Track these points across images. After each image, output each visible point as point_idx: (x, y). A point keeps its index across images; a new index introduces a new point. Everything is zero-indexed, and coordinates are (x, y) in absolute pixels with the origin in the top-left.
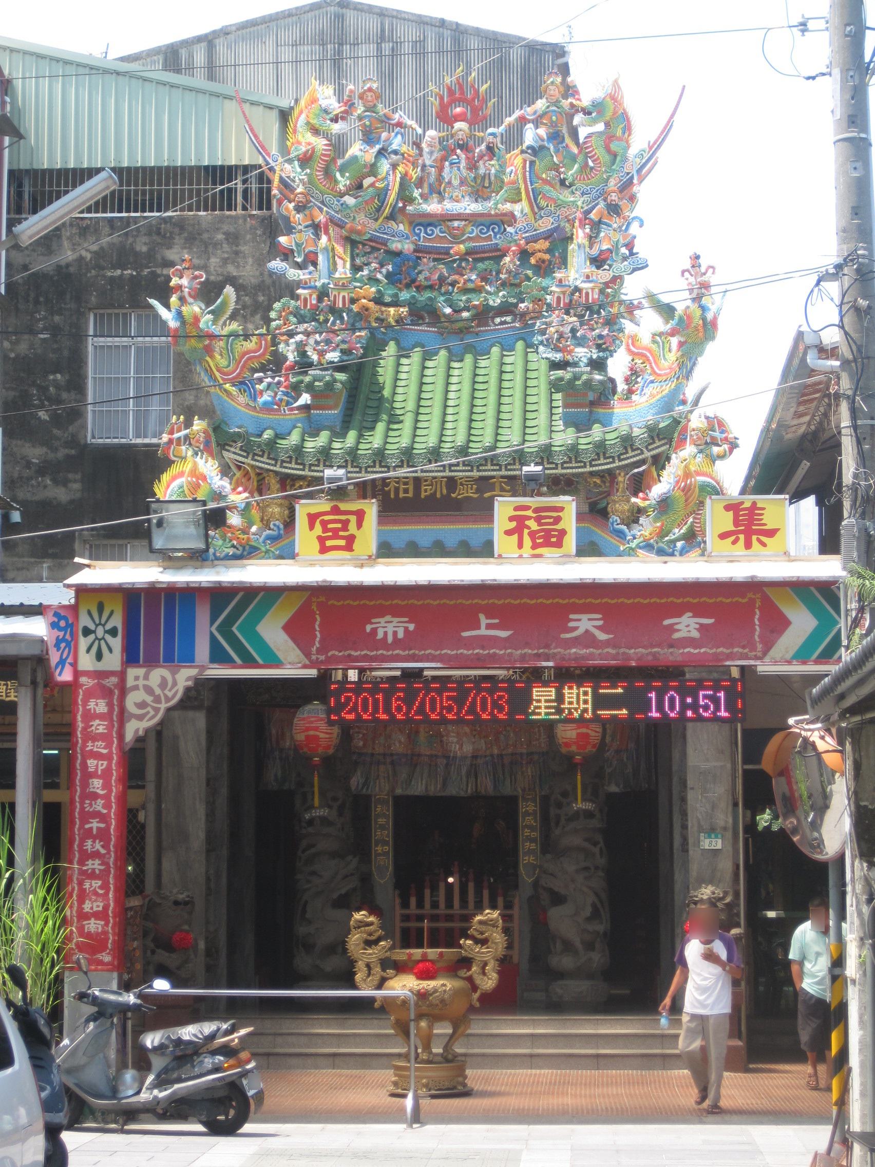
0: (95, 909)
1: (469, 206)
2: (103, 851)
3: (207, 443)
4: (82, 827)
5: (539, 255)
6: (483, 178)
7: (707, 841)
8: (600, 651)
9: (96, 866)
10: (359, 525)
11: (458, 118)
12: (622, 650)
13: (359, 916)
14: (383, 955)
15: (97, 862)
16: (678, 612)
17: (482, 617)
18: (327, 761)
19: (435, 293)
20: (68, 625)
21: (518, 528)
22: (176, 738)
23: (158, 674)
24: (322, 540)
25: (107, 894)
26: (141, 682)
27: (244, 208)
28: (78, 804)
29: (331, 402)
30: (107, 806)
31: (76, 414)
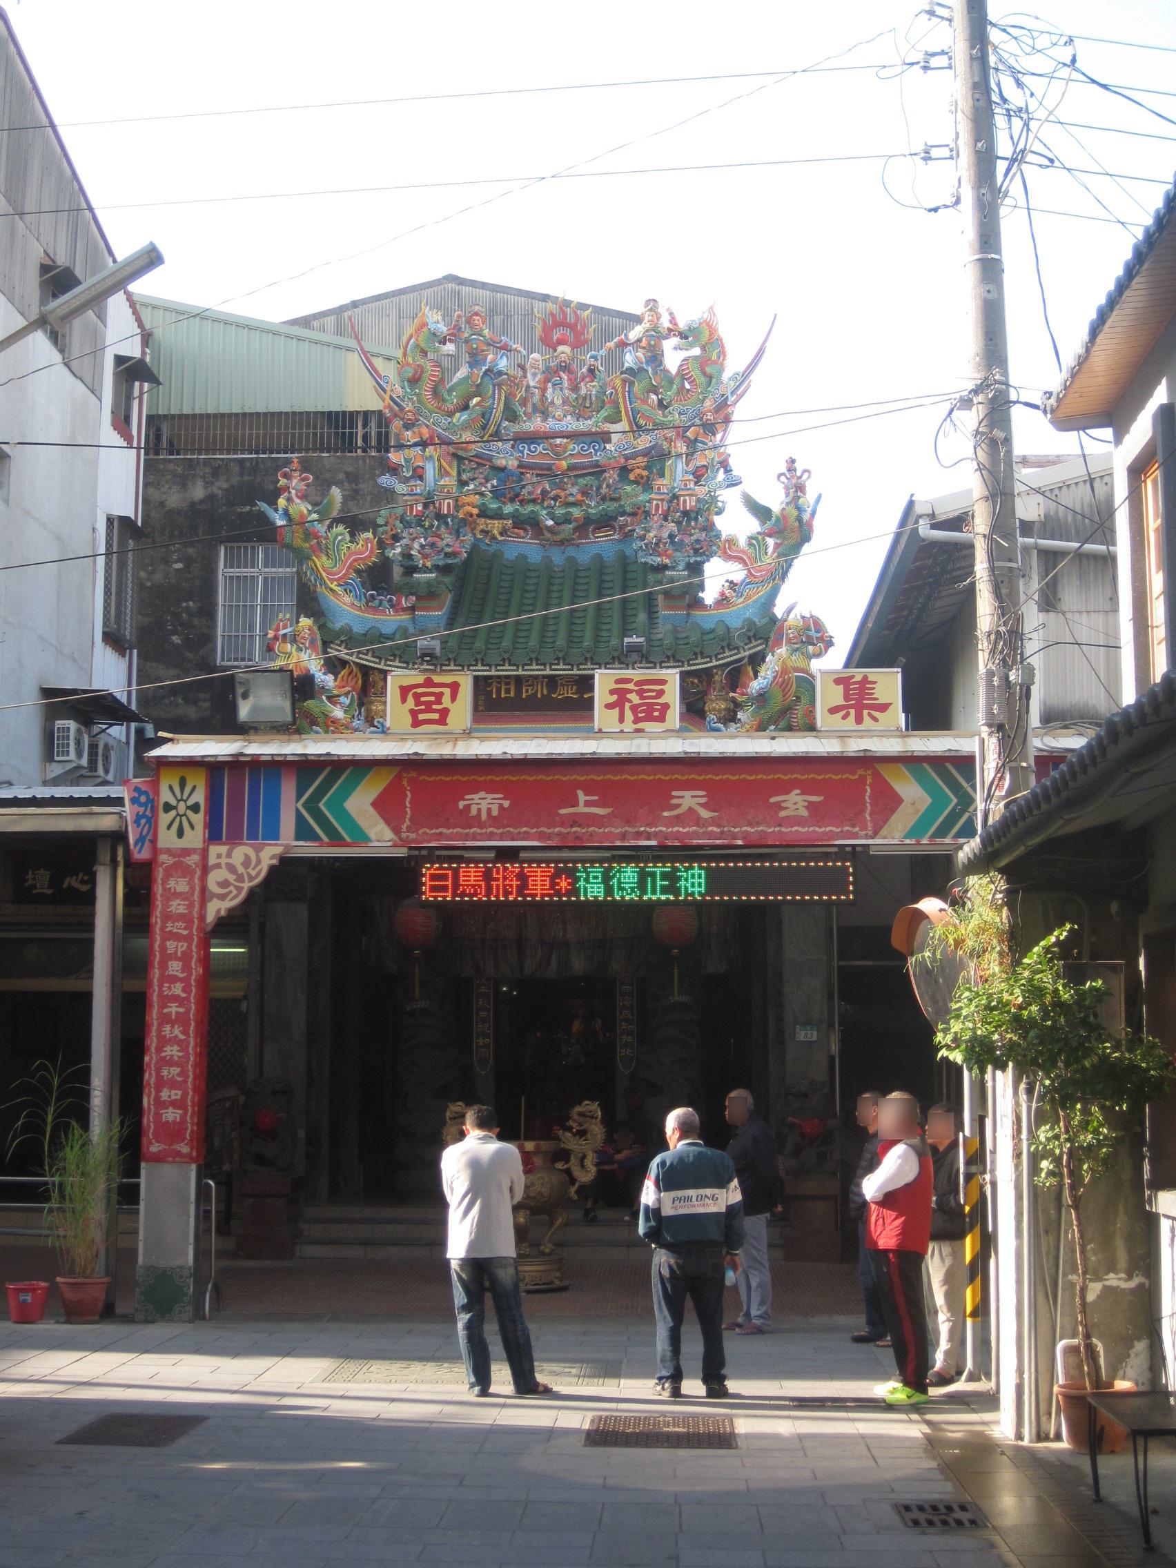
1: (571, 424)
3: (313, 643)
4: (160, 1013)
5: (638, 471)
6: (585, 398)
7: (803, 1033)
9: (175, 1053)
10: (453, 698)
11: (561, 342)
16: (786, 788)
17: (580, 793)
21: (619, 701)
23: (241, 852)
24: (414, 713)
25: (185, 1082)
26: (224, 861)
27: (364, 451)
29: (435, 604)
31: (207, 638)
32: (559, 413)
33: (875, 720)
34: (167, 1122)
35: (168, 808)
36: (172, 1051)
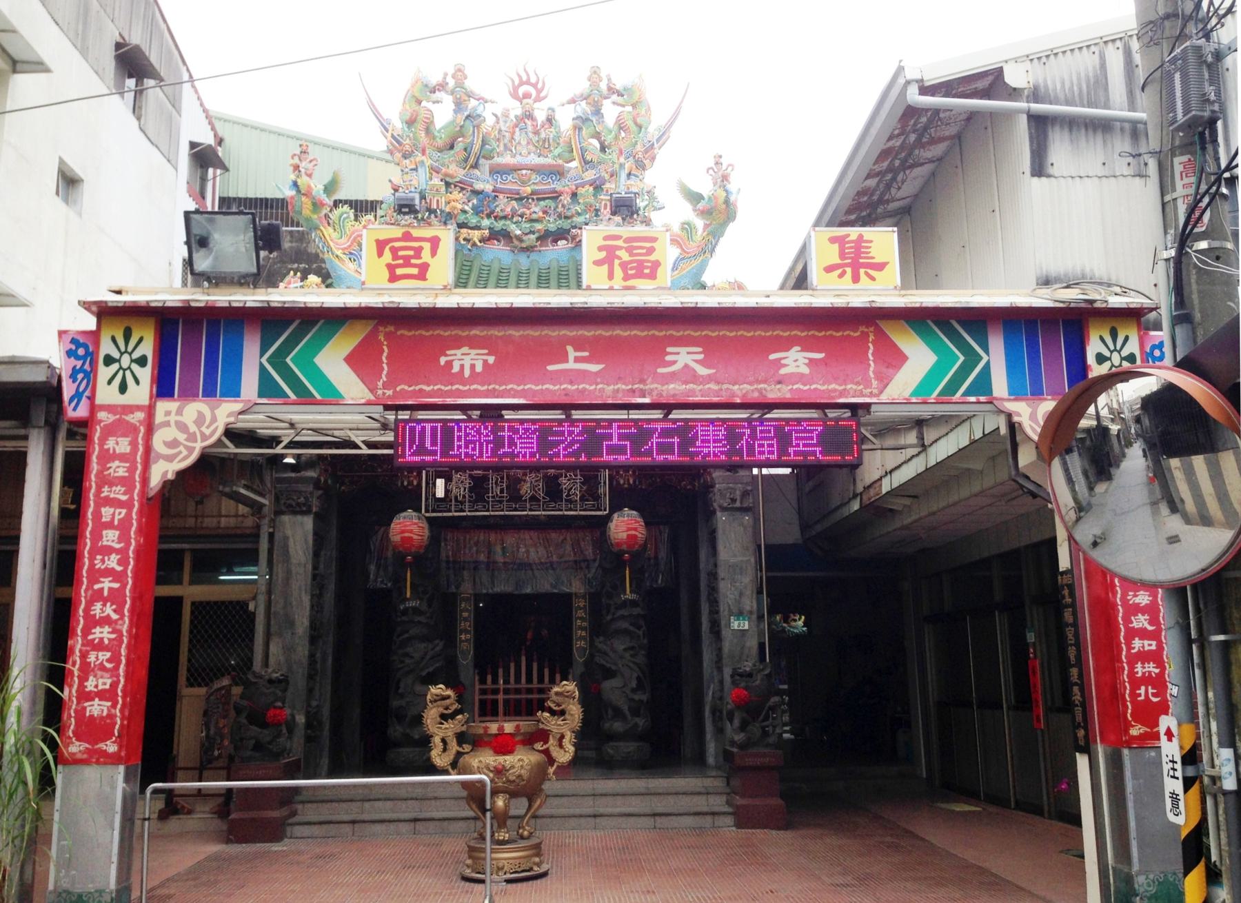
0: (100, 687)
2: (115, 616)
7: (736, 623)
8: (701, 387)
10: (434, 252)
12: (725, 386)
13: (437, 690)
14: (460, 729)
15: (107, 629)
16: (786, 345)
17: (570, 349)
18: (418, 559)
19: (508, 222)
20: (87, 353)
22: (286, 538)
23: (195, 408)
24: (391, 268)
25: (117, 668)
26: (173, 418)
28: (86, 561)
30: (123, 562)
32: (524, 152)
33: (873, 279)
34: (91, 716)
35: (109, 360)
36: (102, 633)
